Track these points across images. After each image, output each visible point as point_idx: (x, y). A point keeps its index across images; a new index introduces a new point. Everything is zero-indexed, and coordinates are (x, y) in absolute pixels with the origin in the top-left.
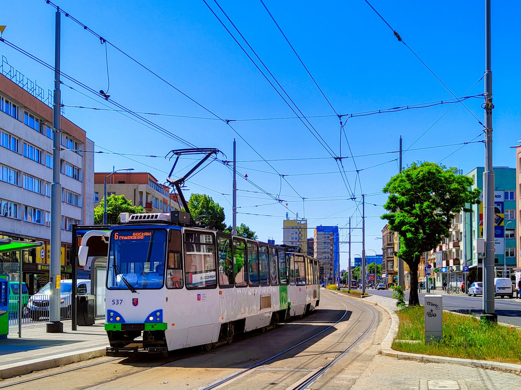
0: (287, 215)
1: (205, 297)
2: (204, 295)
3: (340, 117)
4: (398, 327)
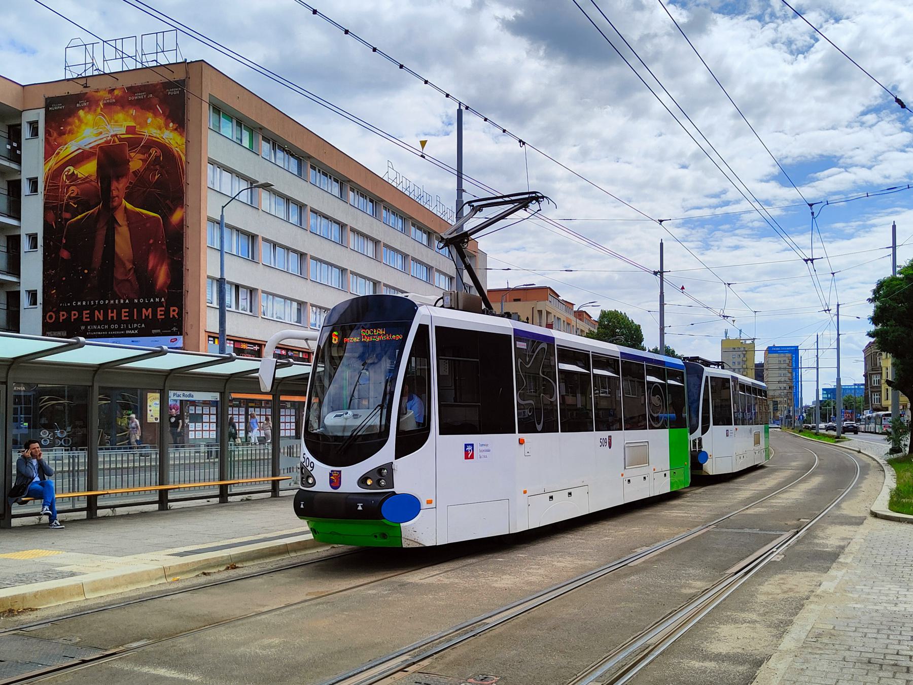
0: (726, 333)
2: (487, 445)
3: (811, 205)
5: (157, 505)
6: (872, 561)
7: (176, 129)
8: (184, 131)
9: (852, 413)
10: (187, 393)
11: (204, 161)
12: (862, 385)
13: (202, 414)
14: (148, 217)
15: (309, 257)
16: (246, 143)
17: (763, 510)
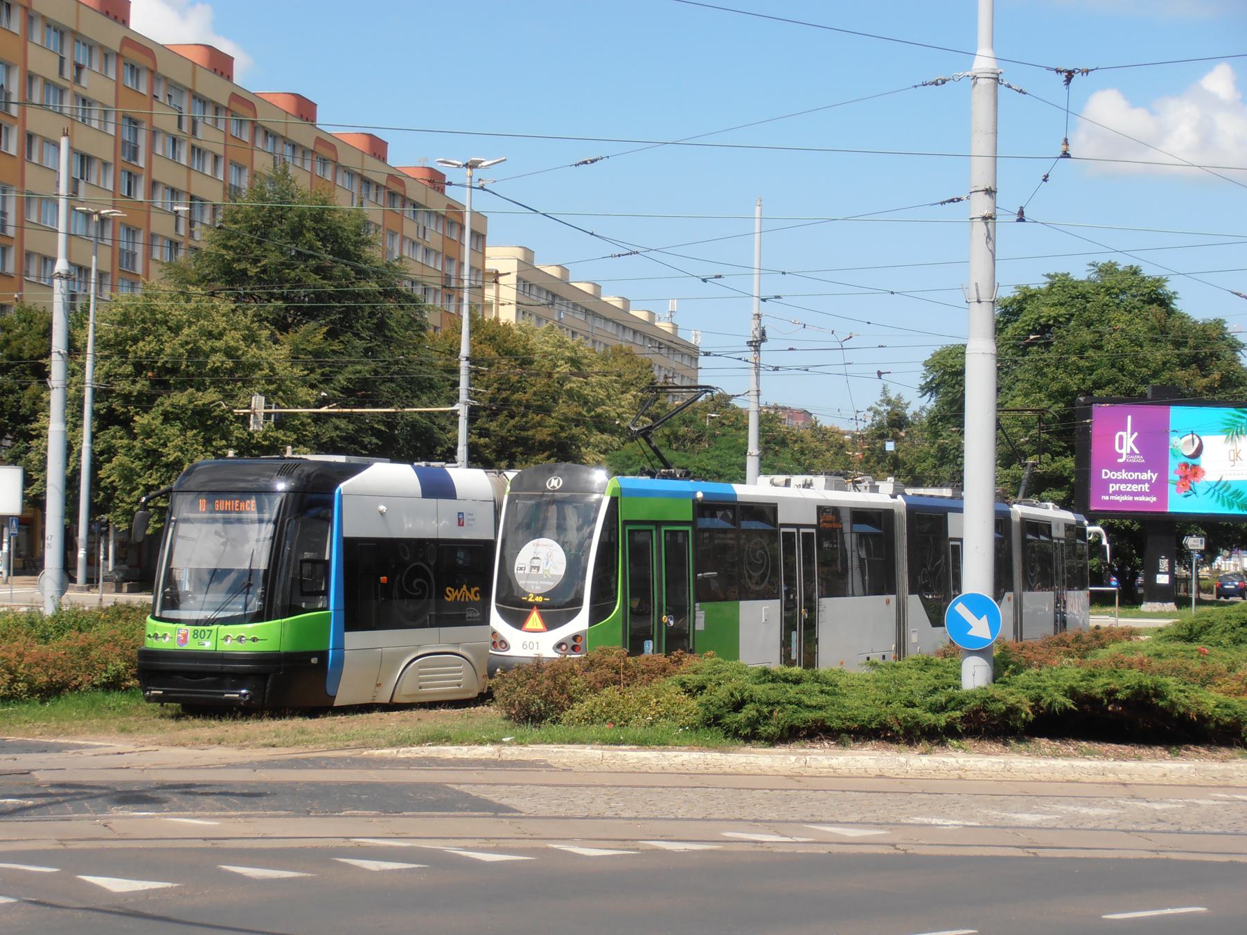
1: (474, 520)
4: (549, 761)
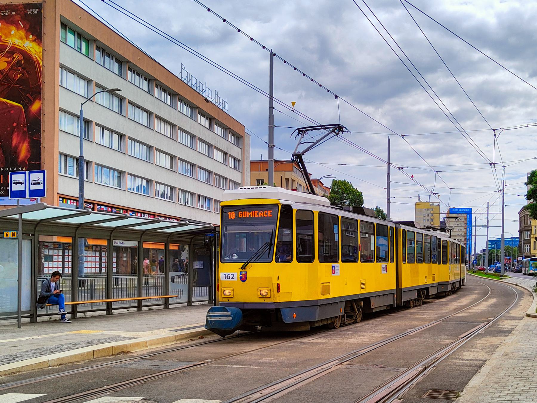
0: (419, 197)
3: (494, 130)
5: (105, 312)
6: (528, 333)
7: (35, 40)
8: (41, 42)
9: (510, 259)
10: (121, 241)
11: (57, 66)
12: (517, 238)
13: (53, 255)
14: (13, 106)
15: (127, 137)
16: (84, 51)
17: (466, 314)
